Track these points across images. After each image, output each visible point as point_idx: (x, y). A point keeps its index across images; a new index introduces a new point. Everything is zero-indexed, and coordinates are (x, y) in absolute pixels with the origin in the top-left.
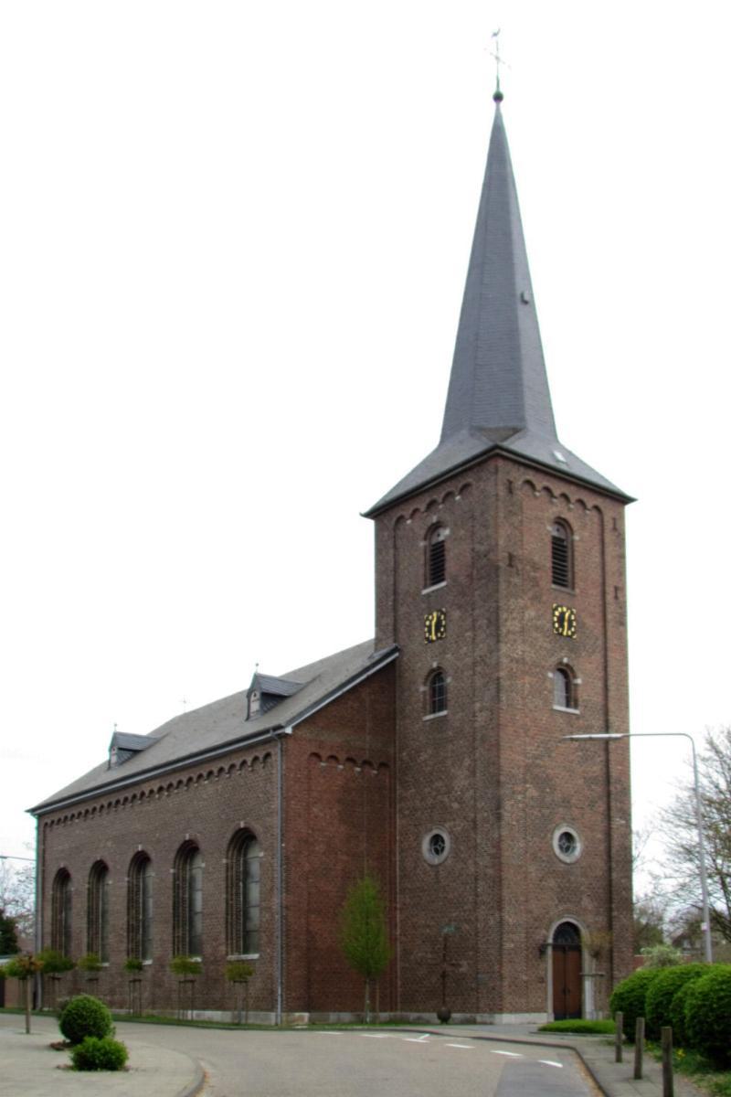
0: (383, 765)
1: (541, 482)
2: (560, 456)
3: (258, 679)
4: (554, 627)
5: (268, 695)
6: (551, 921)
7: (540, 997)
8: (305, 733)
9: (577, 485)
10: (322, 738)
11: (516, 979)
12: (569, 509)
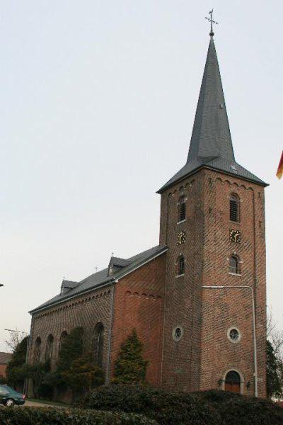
0: (159, 297)
1: (224, 178)
2: (234, 168)
3: (113, 259)
5: (117, 265)
8: (124, 283)
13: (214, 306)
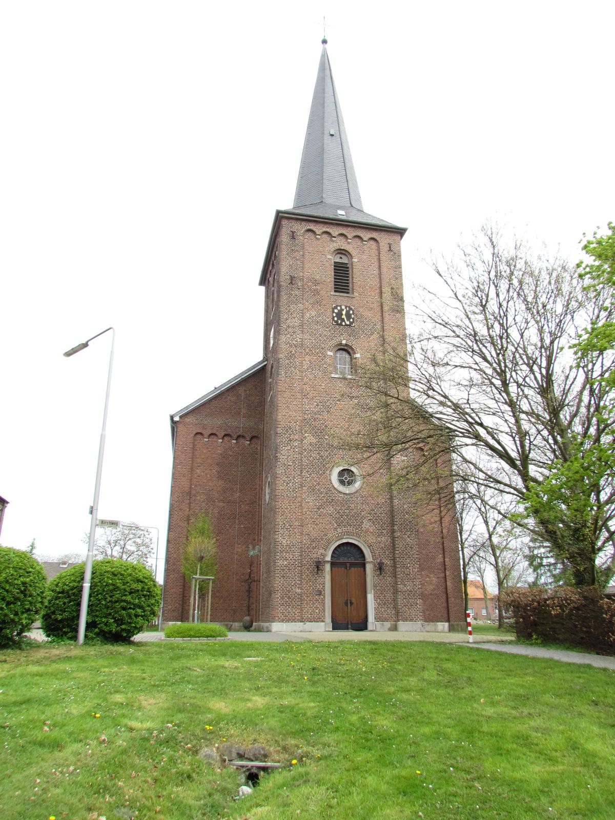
1: (319, 229)
4: (333, 320)
6: (329, 543)
7: (317, 608)
9: (354, 227)
10: (206, 422)
11: (289, 591)
12: (349, 243)
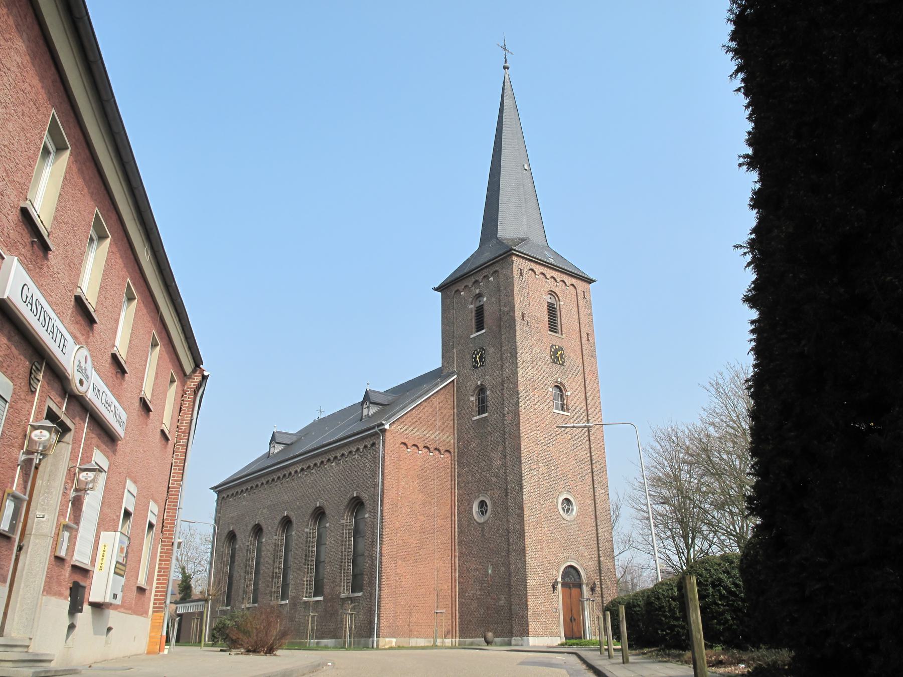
1: (539, 269)
13: (538, 462)
